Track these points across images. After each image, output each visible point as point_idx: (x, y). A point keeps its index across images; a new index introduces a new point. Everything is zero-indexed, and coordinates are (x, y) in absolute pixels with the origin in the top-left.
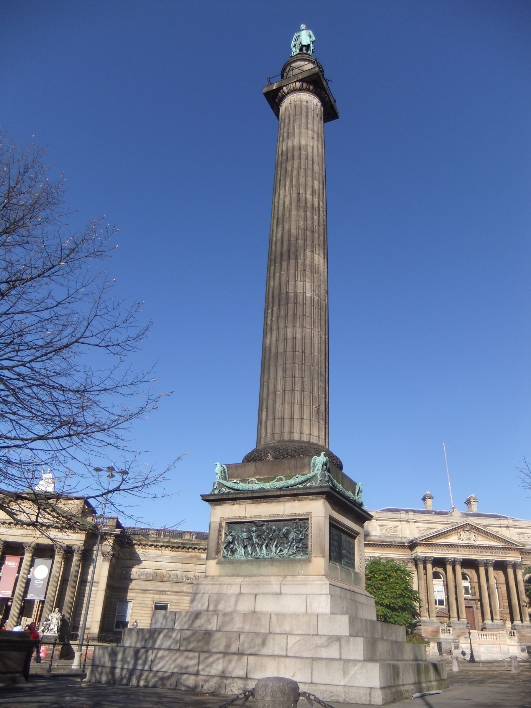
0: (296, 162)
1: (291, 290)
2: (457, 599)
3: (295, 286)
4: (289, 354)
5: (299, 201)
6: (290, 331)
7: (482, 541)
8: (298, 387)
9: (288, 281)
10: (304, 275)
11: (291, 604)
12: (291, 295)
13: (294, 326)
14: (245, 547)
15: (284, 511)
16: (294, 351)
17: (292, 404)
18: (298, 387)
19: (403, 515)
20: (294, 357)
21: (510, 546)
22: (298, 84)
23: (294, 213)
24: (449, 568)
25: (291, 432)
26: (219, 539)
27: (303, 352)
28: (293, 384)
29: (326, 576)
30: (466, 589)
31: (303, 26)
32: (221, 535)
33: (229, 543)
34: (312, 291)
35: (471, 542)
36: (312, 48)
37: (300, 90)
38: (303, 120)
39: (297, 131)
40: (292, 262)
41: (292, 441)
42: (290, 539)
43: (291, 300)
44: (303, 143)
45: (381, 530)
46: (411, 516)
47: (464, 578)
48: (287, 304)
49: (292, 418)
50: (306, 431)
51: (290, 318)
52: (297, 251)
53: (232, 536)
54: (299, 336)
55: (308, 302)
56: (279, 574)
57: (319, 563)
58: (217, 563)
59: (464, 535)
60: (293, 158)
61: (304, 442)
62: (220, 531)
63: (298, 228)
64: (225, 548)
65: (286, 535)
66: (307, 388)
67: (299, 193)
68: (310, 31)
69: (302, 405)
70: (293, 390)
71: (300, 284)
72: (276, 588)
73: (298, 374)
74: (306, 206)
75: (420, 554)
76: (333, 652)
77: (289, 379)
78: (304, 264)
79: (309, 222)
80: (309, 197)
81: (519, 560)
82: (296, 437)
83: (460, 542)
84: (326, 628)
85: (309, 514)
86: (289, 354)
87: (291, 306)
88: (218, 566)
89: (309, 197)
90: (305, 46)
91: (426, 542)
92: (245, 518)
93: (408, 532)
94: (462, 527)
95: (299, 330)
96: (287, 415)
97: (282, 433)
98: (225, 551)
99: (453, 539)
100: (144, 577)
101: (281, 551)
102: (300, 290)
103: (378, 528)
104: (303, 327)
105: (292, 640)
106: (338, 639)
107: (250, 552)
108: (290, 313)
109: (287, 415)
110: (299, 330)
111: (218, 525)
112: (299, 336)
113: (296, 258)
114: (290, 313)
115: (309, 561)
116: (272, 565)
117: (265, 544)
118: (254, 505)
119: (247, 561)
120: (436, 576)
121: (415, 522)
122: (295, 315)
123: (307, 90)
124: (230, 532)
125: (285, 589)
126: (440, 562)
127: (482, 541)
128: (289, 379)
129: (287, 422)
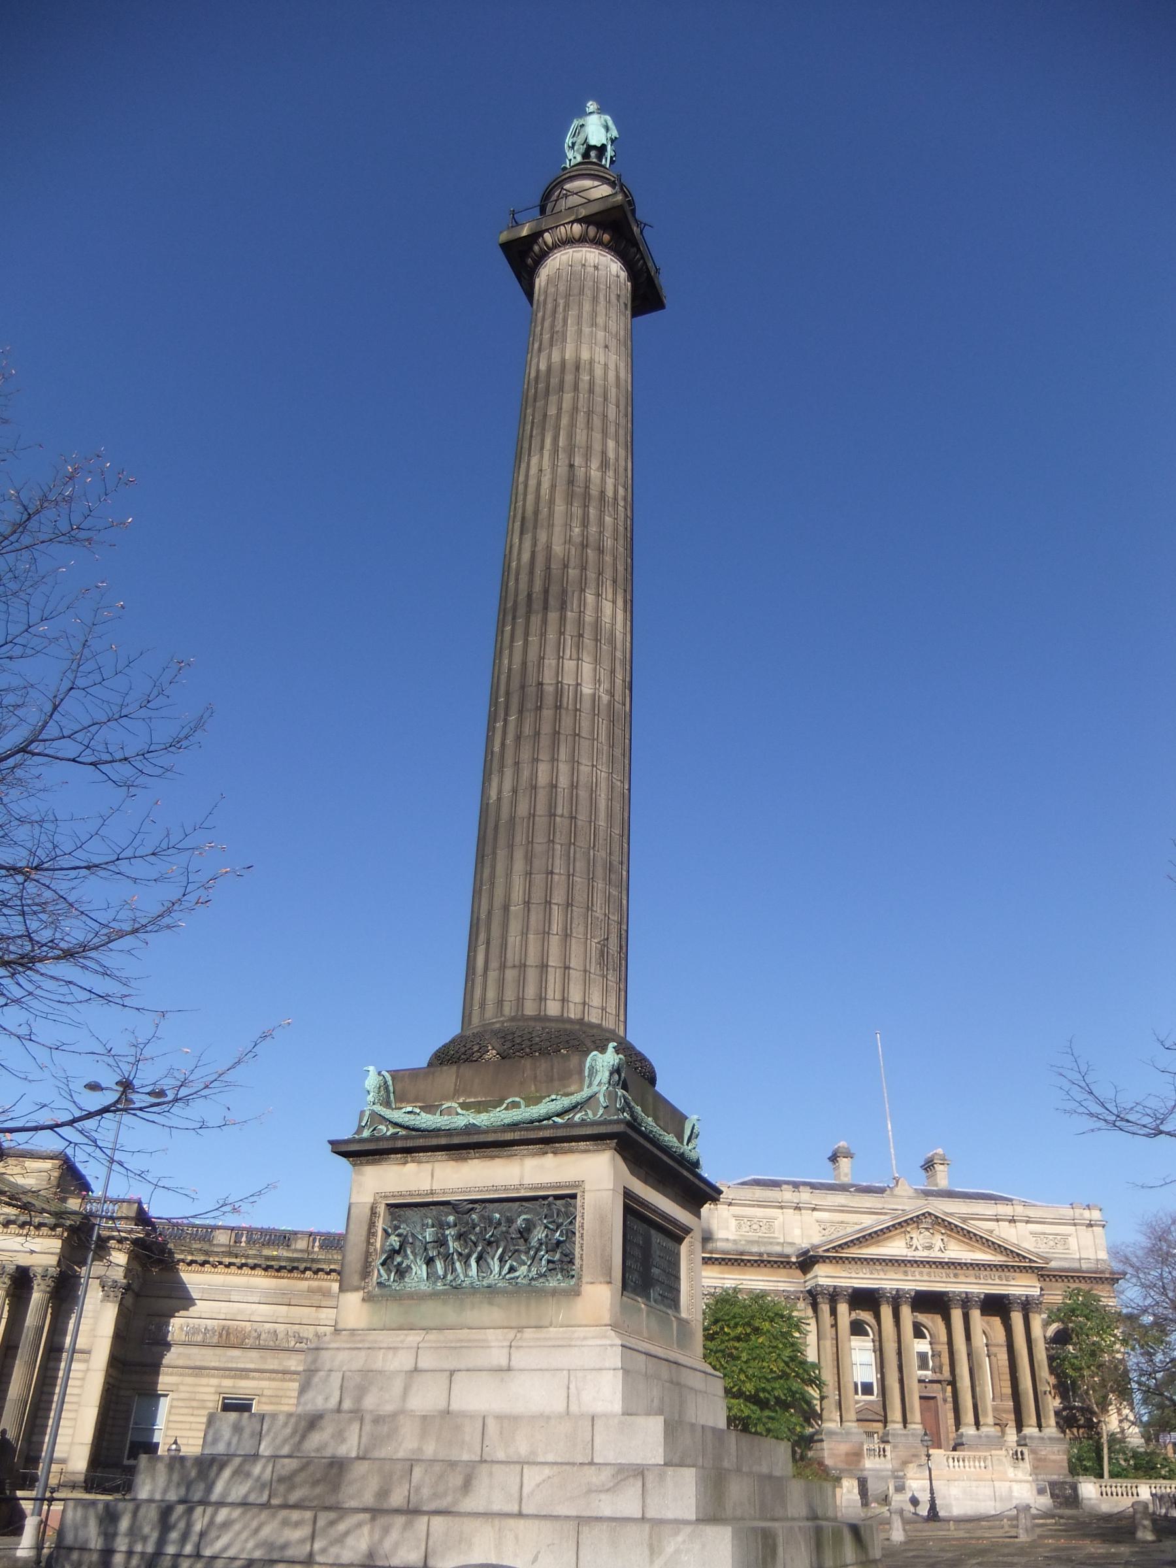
0: (568, 397)
1: (548, 678)
2: (901, 1381)
3: (559, 670)
4: (541, 821)
5: (571, 481)
6: (543, 769)
7: (957, 1251)
8: (558, 897)
9: (541, 658)
10: (579, 647)
11: (533, 1394)
12: (549, 689)
13: (554, 760)
14: (430, 1262)
15: (522, 1177)
16: (552, 815)
17: (545, 933)
18: (558, 897)
19: (787, 1195)
20: (552, 827)
21: (1018, 1262)
22: (577, 228)
23: (560, 508)
24: (886, 1312)
25: (541, 999)
26: (368, 1243)
27: (573, 818)
28: (549, 889)
29: (614, 1326)
30: (923, 1357)
31: (591, 106)
32: (375, 1234)
33: (394, 1252)
34: (597, 681)
35: (935, 1254)
36: (609, 152)
37: (582, 240)
38: (587, 307)
39: (571, 330)
40: (553, 616)
41: (542, 1018)
42: (534, 1243)
43: (549, 700)
44: (585, 355)
45: (739, 1226)
46: (805, 1195)
47: (919, 1334)
48: (539, 708)
49: (543, 967)
50: (575, 995)
51: (545, 741)
52: (564, 592)
53: (399, 1235)
54: (563, 782)
55: (586, 705)
56: (505, 1324)
57: (599, 1296)
58: (363, 1300)
59: (920, 1237)
60: (561, 388)
61: (570, 1021)
62: (372, 1224)
63: (568, 541)
64: (383, 1264)
65: (525, 1233)
66: (580, 897)
67: (571, 466)
68: (608, 118)
69: (566, 936)
70: (548, 903)
71: (570, 665)
72: (498, 1357)
73: (559, 867)
74: (586, 495)
75: (823, 1281)
76: (627, 1503)
77: (538, 879)
78: (580, 622)
79: (593, 529)
80: (595, 474)
81: (1036, 1292)
82: (553, 1009)
83: (910, 1254)
84: (612, 1448)
85: (578, 1184)
86: (541, 821)
87: (547, 713)
88: (366, 1306)
89: (595, 474)
90: (595, 147)
91: (836, 1255)
92: (432, 1193)
93: (797, 1232)
94: (916, 1221)
95: (564, 768)
96: (532, 959)
97: (520, 1000)
98: (382, 1271)
99: (895, 1247)
100: (199, 1338)
101: (512, 1269)
102: (568, 680)
103: (733, 1223)
104: (574, 762)
105: (532, 1477)
106: (640, 1472)
107: (441, 1272)
108: (546, 729)
109: (532, 959)
110: (564, 768)
111: (368, 1211)
112: (563, 782)
113: (563, 607)
114: (546, 729)
115: (576, 1292)
116: (491, 1303)
117: (475, 1255)
118: (452, 1163)
119: (434, 1295)
120: (858, 1329)
121: (814, 1209)
122: (556, 734)
123: (596, 242)
124: (397, 1228)
125: (519, 1359)
126: (865, 1299)
127: (957, 1251)
128: (538, 879)
129: (532, 975)
